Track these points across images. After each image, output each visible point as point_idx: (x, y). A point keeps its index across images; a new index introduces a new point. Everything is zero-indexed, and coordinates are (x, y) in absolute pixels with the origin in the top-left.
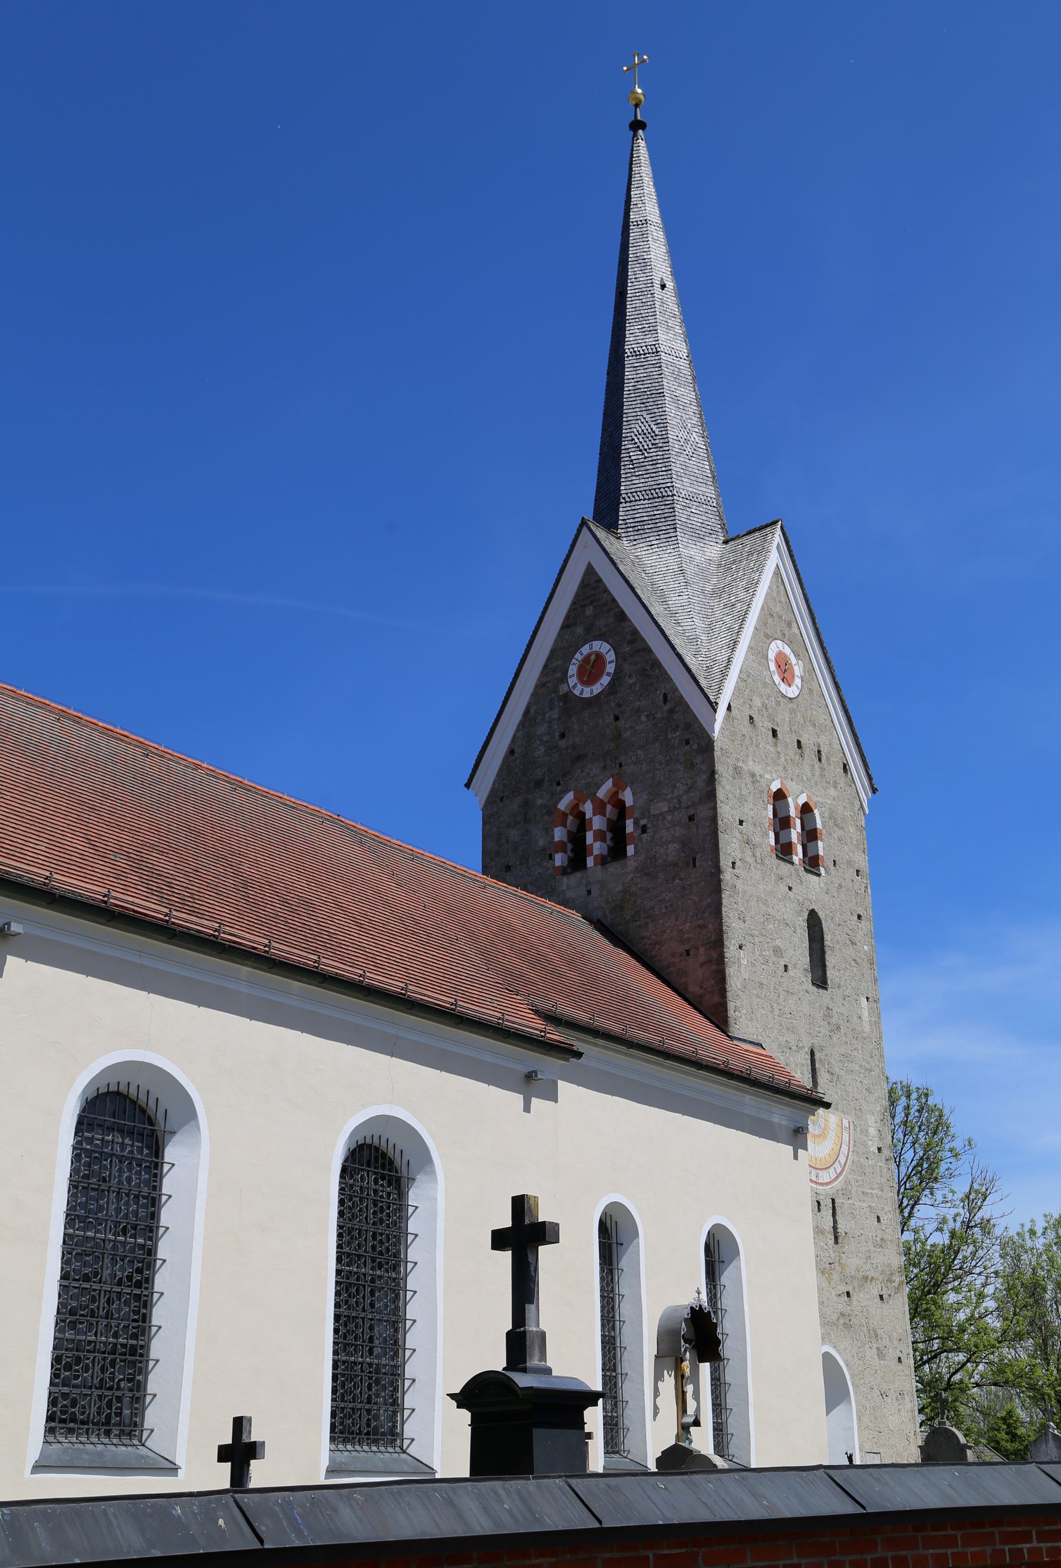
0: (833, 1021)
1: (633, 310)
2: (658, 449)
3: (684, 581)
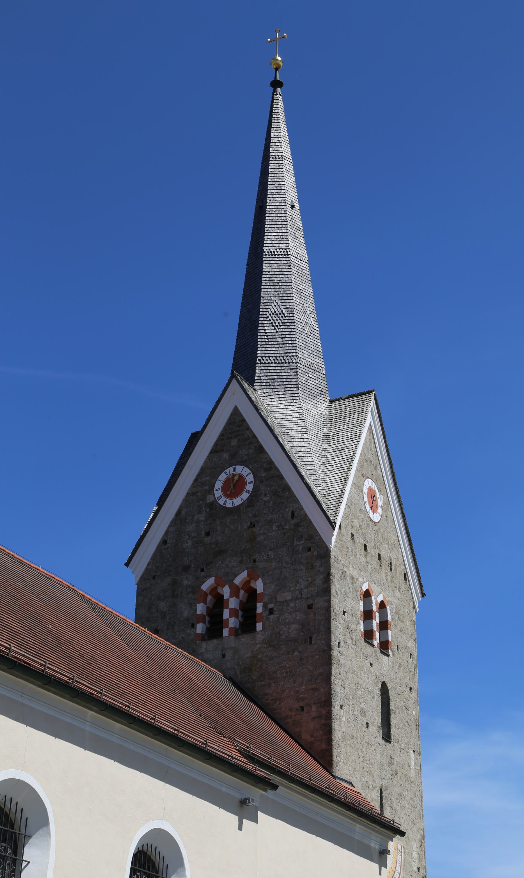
0: (394, 767)
1: (270, 221)
2: (286, 327)
3: (305, 427)
